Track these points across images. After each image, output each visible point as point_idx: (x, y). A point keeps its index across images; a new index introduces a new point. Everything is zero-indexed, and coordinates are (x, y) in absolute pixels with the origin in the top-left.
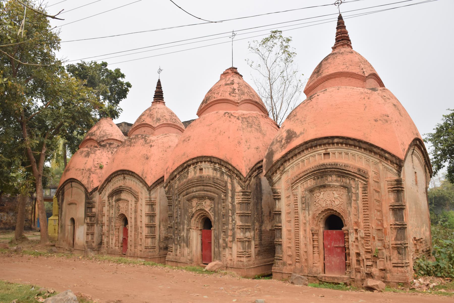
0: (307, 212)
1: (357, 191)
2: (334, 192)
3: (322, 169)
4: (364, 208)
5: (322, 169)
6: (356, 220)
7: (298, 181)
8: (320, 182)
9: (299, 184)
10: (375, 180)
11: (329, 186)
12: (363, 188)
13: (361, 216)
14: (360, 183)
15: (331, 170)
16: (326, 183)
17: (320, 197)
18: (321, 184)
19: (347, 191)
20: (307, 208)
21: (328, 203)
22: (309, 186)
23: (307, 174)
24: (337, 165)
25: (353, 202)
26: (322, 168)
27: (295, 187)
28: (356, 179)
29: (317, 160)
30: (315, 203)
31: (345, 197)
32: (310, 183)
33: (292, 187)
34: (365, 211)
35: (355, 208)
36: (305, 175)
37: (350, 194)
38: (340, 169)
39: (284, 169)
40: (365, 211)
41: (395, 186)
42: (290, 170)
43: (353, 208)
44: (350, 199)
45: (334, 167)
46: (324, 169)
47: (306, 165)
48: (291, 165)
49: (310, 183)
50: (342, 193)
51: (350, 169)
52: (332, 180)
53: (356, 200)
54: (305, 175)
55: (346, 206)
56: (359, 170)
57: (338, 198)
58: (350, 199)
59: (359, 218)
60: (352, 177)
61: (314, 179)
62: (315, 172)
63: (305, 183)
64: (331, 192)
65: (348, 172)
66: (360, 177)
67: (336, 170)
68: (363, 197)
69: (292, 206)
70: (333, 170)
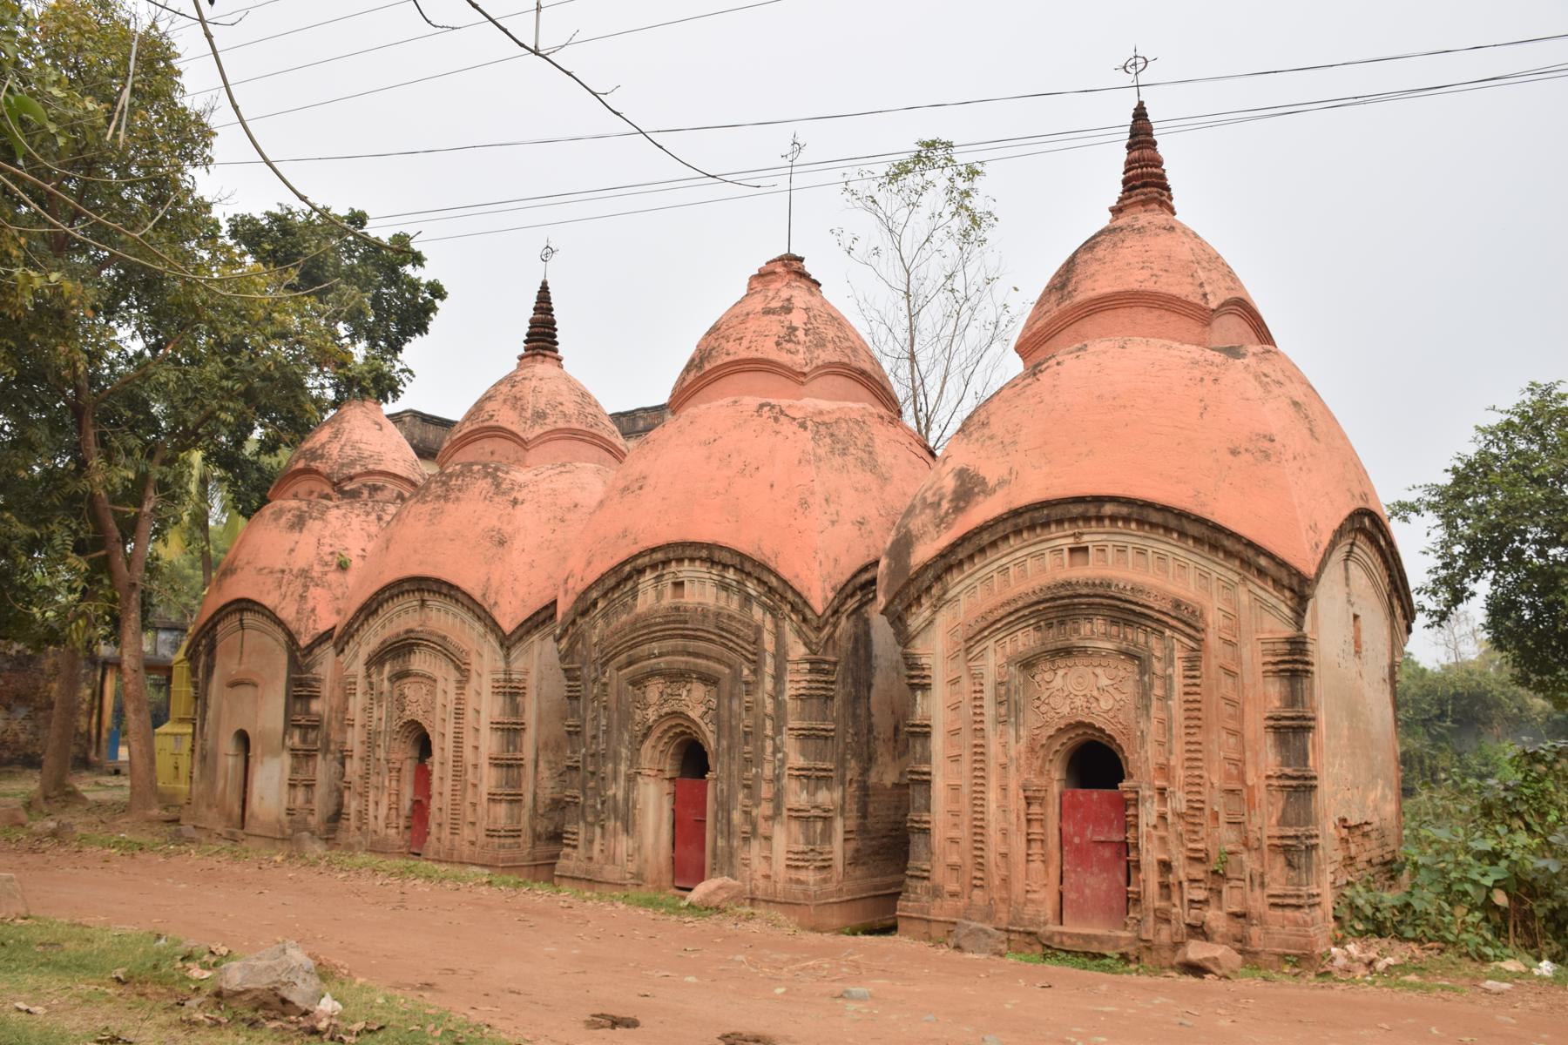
0: (1012, 732)
1: (1170, 671)
2: (1099, 671)
3: (1062, 598)
5: (1062, 598)
6: (1162, 760)
8: (1054, 638)
9: (990, 643)
10: (1223, 635)
12: (1188, 659)
13: (1179, 747)
14: (1177, 646)
18: (1059, 645)
21: (1078, 703)
23: (1017, 611)
24: (1109, 586)
25: (1154, 703)
26: (1063, 593)
27: (976, 650)
28: (1168, 632)
30: (1037, 703)
31: (1130, 687)
32: (1025, 640)
33: (968, 650)
35: (1161, 721)
36: (1011, 614)
42: (962, 597)
45: (1100, 591)
48: (968, 582)
49: (1025, 640)
50: (1122, 673)
54: (1011, 614)
55: (1133, 715)
56: (1177, 604)
58: (1145, 693)
59: (1170, 753)
61: (1038, 628)
62: (1041, 607)
64: (1090, 670)
66: (1180, 626)
69: (967, 710)
70: (1098, 600)
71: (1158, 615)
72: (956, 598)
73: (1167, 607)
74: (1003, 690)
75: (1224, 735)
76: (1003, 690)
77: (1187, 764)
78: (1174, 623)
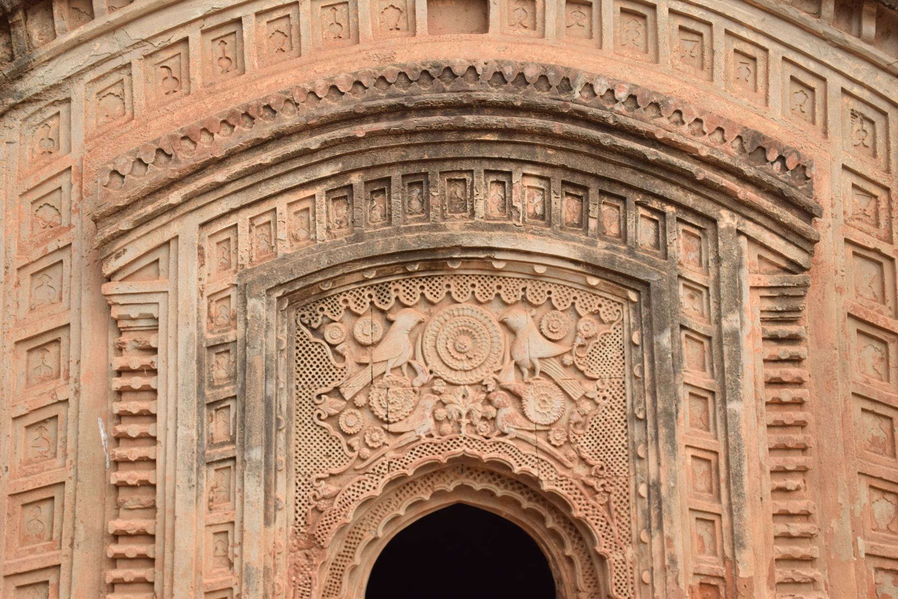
0: (254, 490)
1: (730, 322)
2: (520, 318)
3: (426, 109)
4: (779, 460)
5: (426, 109)
6: (711, 564)
7: (175, 197)
9: (186, 228)
10: (858, 237)
11: (482, 259)
12: (779, 293)
13: (757, 524)
14: (750, 254)
15: (516, 121)
16: (456, 229)
17: (379, 353)
18: (411, 240)
19: (628, 315)
20: (257, 454)
21: (458, 405)
22: (284, 248)
24: (567, 85)
25: (688, 409)
26: (426, 94)
27: (135, 248)
28: (727, 219)
29: (367, 30)
30: (330, 405)
31: (609, 366)
32: (301, 225)
33: (104, 249)
34: (791, 483)
35: (705, 457)
36: (260, 145)
37: (665, 339)
38: (601, 125)
39: (19, 75)
40: (791, 483)
41: (705, 300)
42: (78, 91)
43: (685, 456)
44: (656, 377)
45: (541, 97)
46: (448, 107)
47: (251, 61)
48: (102, 47)
49: (301, 225)
50: (588, 325)
51: (683, 135)
52: (507, 205)
53: (718, 394)
54: (260, 145)
55: (618, 440)
56: (758, 146)
57: (555, 369)
58: (656, 377)
59: (737, 542)
60: (690, 200)
61: (343, 193)
62: (360, 130)
63: (242, 219)
64: (494, 312)
65: (664, 156)
66: (766, 203)
67: (558, 127)
68: (775, 372)
69: (90, 427)
70: (534, 122)
71: (704, 173)
72: (57, 96)
73: (729, 153)
74: (221, 367)
75: (864, 492)
76: (221, 367)
77: (783, 573)
78: (746, 193)
